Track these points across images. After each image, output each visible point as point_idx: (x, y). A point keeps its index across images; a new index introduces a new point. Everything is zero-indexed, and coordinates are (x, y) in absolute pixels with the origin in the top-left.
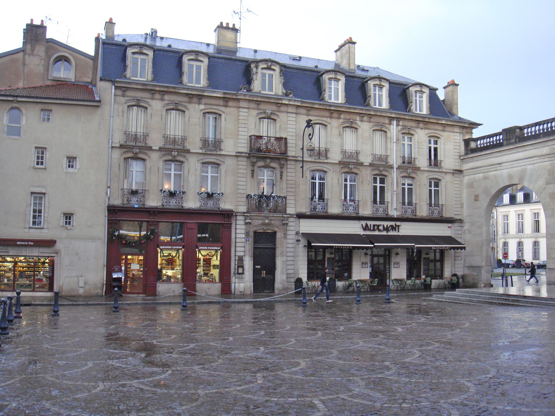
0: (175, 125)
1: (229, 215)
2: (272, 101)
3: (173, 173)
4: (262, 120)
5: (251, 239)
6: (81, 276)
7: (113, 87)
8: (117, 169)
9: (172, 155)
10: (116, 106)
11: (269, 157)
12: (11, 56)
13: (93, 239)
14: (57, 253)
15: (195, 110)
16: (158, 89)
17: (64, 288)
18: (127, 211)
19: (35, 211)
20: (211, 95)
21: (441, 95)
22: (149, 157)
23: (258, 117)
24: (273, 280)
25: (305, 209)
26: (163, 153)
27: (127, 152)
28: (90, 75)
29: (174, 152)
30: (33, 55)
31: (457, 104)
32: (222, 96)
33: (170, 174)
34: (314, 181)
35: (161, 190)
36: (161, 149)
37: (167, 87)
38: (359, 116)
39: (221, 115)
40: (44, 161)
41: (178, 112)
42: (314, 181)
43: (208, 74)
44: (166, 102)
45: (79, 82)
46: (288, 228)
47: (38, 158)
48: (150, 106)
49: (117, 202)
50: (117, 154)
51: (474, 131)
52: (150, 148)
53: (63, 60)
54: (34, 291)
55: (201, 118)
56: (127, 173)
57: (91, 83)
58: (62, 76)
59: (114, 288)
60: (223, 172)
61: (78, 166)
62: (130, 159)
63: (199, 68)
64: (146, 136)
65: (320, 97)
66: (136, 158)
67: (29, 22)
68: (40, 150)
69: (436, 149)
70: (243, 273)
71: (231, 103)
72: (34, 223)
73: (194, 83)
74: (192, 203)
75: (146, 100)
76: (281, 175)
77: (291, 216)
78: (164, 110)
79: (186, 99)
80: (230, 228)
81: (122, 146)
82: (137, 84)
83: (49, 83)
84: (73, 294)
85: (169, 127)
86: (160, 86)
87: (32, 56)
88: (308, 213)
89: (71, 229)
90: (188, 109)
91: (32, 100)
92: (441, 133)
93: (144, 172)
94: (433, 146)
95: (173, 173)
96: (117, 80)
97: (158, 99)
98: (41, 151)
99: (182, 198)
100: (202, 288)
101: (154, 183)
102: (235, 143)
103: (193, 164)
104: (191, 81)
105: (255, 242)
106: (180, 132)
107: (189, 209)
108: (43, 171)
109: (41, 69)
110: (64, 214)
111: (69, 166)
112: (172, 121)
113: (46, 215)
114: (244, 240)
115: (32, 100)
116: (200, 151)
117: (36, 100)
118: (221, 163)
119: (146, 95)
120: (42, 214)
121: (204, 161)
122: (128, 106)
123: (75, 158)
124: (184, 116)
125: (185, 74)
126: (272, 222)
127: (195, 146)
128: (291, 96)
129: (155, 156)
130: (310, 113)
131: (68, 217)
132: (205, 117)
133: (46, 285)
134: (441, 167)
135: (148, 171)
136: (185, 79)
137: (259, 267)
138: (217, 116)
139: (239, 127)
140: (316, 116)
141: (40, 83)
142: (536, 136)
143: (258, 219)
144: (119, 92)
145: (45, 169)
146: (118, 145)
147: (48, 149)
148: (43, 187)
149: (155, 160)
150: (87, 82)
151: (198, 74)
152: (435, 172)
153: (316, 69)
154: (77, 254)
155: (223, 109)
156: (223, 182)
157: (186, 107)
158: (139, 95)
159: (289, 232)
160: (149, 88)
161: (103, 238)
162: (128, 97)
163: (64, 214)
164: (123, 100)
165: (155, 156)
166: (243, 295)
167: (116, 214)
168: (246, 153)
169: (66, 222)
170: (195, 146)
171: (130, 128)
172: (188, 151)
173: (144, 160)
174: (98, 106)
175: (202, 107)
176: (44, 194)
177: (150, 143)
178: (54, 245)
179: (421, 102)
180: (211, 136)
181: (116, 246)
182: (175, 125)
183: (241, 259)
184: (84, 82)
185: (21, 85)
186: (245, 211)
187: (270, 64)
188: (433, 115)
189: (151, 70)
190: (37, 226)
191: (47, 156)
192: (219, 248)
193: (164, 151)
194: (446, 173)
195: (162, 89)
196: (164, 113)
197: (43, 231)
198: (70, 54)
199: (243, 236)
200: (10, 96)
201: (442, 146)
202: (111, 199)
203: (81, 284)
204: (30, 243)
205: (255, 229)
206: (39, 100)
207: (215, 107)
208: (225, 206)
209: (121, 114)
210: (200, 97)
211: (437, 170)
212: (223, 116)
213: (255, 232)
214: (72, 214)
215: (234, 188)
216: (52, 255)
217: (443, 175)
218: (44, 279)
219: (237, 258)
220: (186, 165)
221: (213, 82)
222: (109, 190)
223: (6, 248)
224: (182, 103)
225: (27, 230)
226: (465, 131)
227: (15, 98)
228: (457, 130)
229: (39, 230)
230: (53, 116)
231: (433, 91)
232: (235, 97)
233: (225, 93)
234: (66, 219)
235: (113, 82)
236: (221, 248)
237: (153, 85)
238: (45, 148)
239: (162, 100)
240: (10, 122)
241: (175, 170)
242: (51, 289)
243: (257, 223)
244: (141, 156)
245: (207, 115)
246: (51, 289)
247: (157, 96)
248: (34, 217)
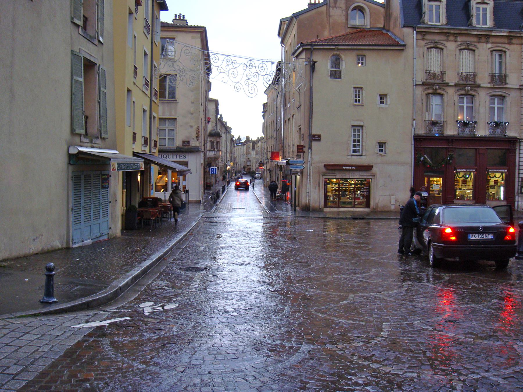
0: (466, 63)
3: (465, 105)
4: (461, 51)
6: (393, 195)
7: (415, 32)
8: (420, 104)
9: (433, 89)
10: (418, 49)
12: (317, 10)
13: (402, 164)
14: (374, 176)
15: (484, 49)
16: (452, 32)
17: (379, 205)
19: (354, 141)
20: (498, 34)
22: (447, 92)
26: (457, 88)
27: (427, 88)
28: (382, 21)
29: (467, 87)
30: (336, 7)
33: (463, 107)
35: (457, 121)
36: (456, 85)
37: (460, 30)
38: (453, 36)
39: (505, 52)
40: (361, 99)
41: (469, 51)
43: (494, 15)
44: (459, 43)
45: (373, 28)
47: (356, 97)
48: (446, 47)
49: (421, 131)
50: (419, 92)
52: (447, 85)
53: (358, 10)
54: (354, 207)
55: (489, 55)
56: (428, 108)
57: (384, 28)
58: (358, 24)
60: (508, 103)
61: (389, 102)
62: (430, 95)
63: (485, 10)
64: (443, 74)
65: (420, 20)
66: (435, 94)
68: (358, 89)
71: (514, 41)
72: (354, 151)
73: (434, 21)
74: (482, 131)
75: (442, 42)
78: (458, 51)
79: (475, 39)
80: (515, 153)
81: (424, 84)
82: (435, 28)
83: (348, 31)
84: (386, 210)
86: (454, 29)
87: (335, 8)
89: (384, 156)
90: (478, 48)
91: (350, 48)
93: (442, 106)
95: (465, 105)
96: (419, 26)
97: (452, 41)
98: (358, 90)
99: (474, 127)
101: (451, 115)
103: (483, 98)
104: (478, 23)
106: (464, 68)
107: (480, 137)
108: (361, 107)
109: (343, 19)
110: (378, 143)
111: (381, 103)
112: (464, 61)
113: (364, 144)
115: (350, 48)
116: (489, 85)
117: (353, 48)
118: (507, 95)
119: (443, 37)
120: (360, 144)
121: (492, 94)
122: (428, 48)
123: (386, 95)
124: (474, 54)
125: (474, 16)
127: (484, 80)
129: (451, 91)
131: (381, 145)
132: (492, 54)
133: (363, 202)
135: (445, 104)
136: (474, 21)
138: (502, 53)
141: (343, 33)
144: (420, 37)
145: (362, 105)
146: (421, 83)
147: (364, 89)
148: (361, 121)
149: (451, 94)
150: (380, 28)
151: (485, 16)
152: (499, 88)
154: (389, 176)
155: (507, 46)
157: (475, 46)
158: (437, 38)
160: (445, 31)
161: (410, 163)
162: (426, 40)
163: (378, 143)
164: (423, 43)
165: (451, 91)
169: (380, 150)
170: (484, 80)
172: (479, 86)
173: (441, 95)
174: (403, 50)
175: (489, 45)
176: (362, 126)
177: (447, 80)
178: (371, 169)
180: (497, 72)
181: (421, 170)
182: (466, 63)
184: (377, 28)
185: (326, 34)
189: (445, 15)
190: (356, 154)
191: (364, 95)
192: (474, 170)
193: (459, 86)
195: (456, 32)
196: (458, 52)
197: (362, 157)
198: (365, 4)
202: (416, 130)
203: (393, 202)
204: (353, 168)
206: (355, 47)
207: (500, 45)
208: (511, 133)
209: (422, 56)
210: (488, 37)
212: (508, 53)
214: (385, 143)
216: (370, 177)
218: (361, 198)
219: (520, 180)
220: (477, 99)
221: (498, 23)
222: (414, 122)
223: (333, 172)
224: (472, 43)
225: (349, 157)
227: (337, 47)
229: (359, 157)
232: (519, 35)
233: (510, 32)
234: (380, 147)
235: (414, 28)
236: (476, 170)
237: (448, 29)
238: (362, 88)
239: (456, 41)
240: (332, 67)
241: (467, 103)
242: (368, 205)
244: (440, 91)
245: (494, 53)
246: (368, 205)
247: (451, 38)
248: (354, 146)
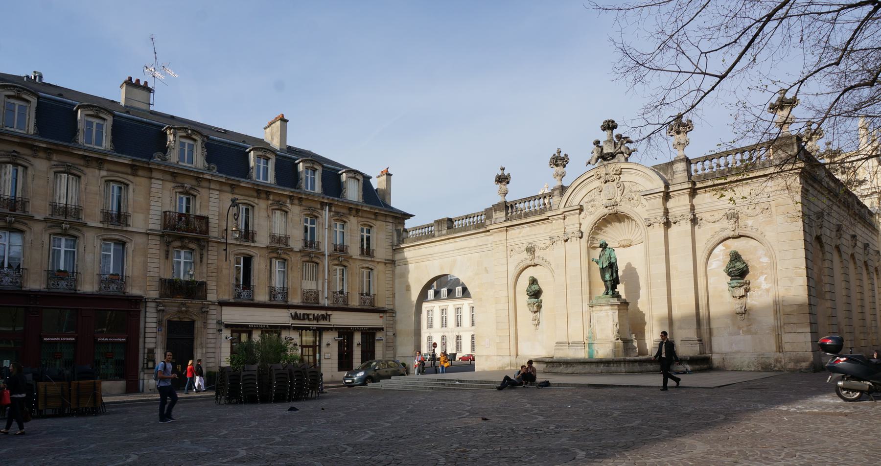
1: (138, 302)
21: (377, 183)
26: (49, 224)
31: (390, 194)
44: (53, 163)
51: (406, 221)
69: (368, 239)
92: (374, 222)
94: (365, 234)
121: (105, 237)
134: (373, 257)
142: (465, 228)
179: (313, 180)
183: (151, 351)
186: (157, 296)
188: (42, 137)
194: (378, 262)
201: (375, 235)
207: (120, 175)
208: (134, 291)
211: (369, 259)
215: (145, 269)
217: (375, 264)
226: (397, 221)
228: (389, 219)
231: (366, 179)
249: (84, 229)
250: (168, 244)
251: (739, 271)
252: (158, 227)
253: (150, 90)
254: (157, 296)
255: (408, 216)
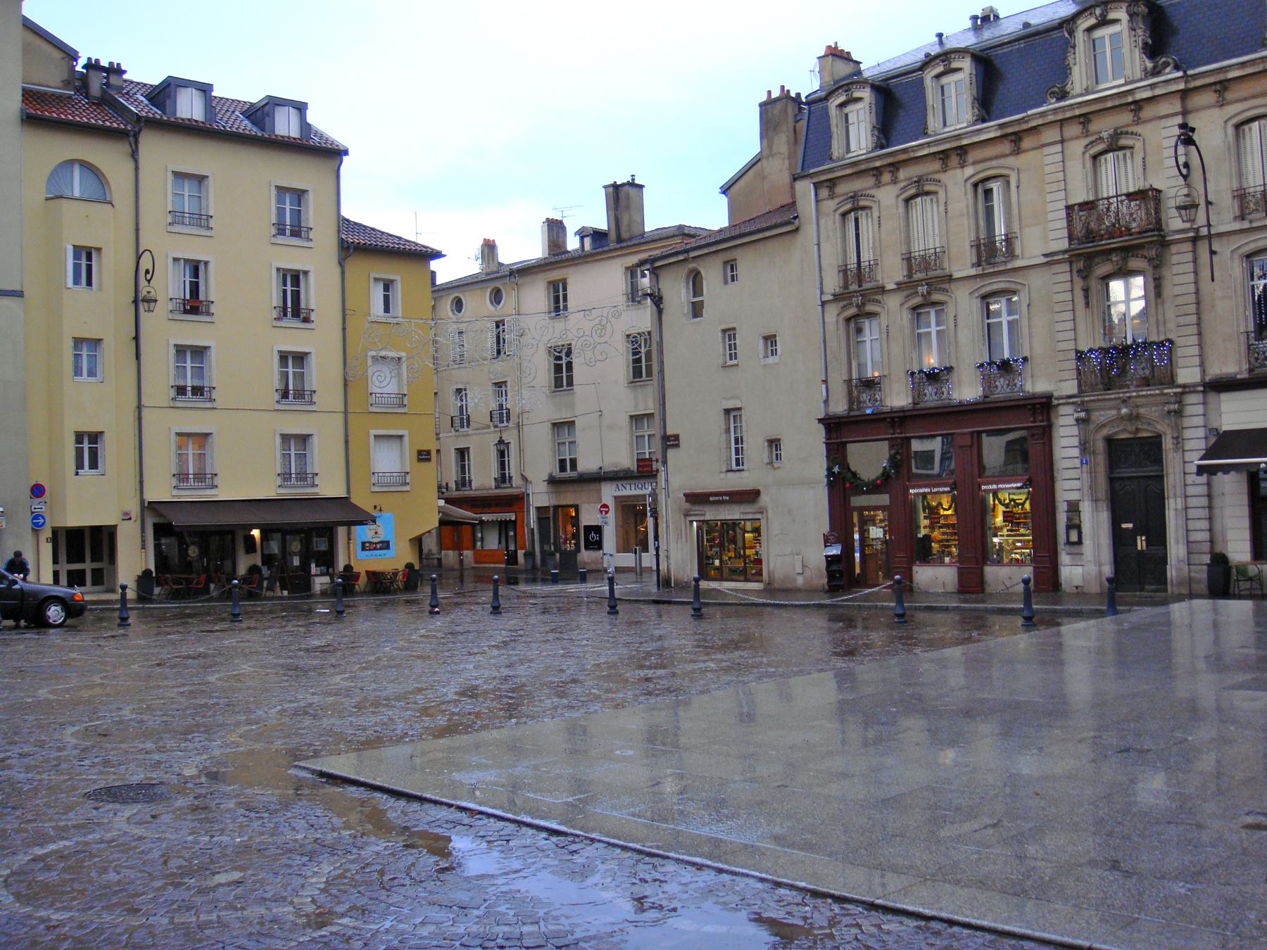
1: (1044, 406)
2: (1109, 104)
5: (1101, 461)
11: (1114, 249)
18: (856, 422)
23: (1087, 155)
24: (1164, 560)
25: (1231, 364)
26: (906, 293)
29: (926, 285)
32: (998, 134)
34: (1011, 318)
42: (1011, 318)
44: (902, 185)
46: (1186, 422)
49: (839, 407)
54: (746, 580)
59: (840, 575)
67: (764, 98)
70: (1080, 542)
76: (1086, 297)
77: (1188, 389)
85: (1250, 168)
88: (1245, 375)
91: (706, 251)
100: (995, 575)
101: (893, 357)
102: (1044, 235)
105: (1112, 464)
107: (961, 404)
114: (1077, 463)
115: (706, 251)
118: (1019, 287)
121: (983, 291)
123: (775, 336)
126: (1142, 410)
128: (1168, 70)
130: (1229, 96)
137: (1130, 526)
139: (1046, 190)
140: (1246, 99)
143: (1104, 409)
153: (1028, 30)
156: (1025, 330)
159: (1188, 434)
164: (830, 205)
166: (1080, 593)
167: (838, 430)
168: (1065, 252)
171: (1251, 177)
172: (950, 278)
183: (1074, 508)
186: (1075, 391)
187: (1098, 11)
199: (1076, 452)
200: (677, 253)
202: (831, 403)
205: (1105, 432)
207: (994, 163)
208: (1036, 384)
213: (1109, 441)
215: (1047, 344)
220: (950, 310)
225: (723, 476)
230: (741, 270)
233: (1001, 126)
243: (1109, 415)
249: (953, 286)
250: (1085, 274)
251: (1187, 137)
252: (1064, 244)
253: (333, 154)
254: (1075, 391)
255: (437, 255)
